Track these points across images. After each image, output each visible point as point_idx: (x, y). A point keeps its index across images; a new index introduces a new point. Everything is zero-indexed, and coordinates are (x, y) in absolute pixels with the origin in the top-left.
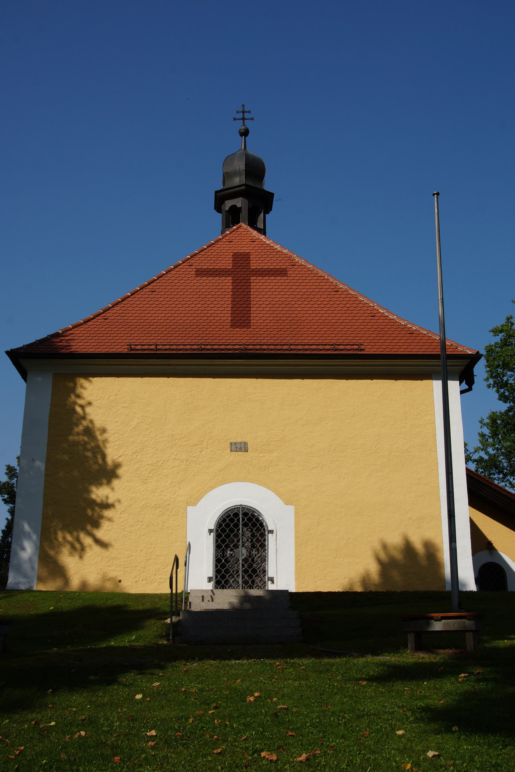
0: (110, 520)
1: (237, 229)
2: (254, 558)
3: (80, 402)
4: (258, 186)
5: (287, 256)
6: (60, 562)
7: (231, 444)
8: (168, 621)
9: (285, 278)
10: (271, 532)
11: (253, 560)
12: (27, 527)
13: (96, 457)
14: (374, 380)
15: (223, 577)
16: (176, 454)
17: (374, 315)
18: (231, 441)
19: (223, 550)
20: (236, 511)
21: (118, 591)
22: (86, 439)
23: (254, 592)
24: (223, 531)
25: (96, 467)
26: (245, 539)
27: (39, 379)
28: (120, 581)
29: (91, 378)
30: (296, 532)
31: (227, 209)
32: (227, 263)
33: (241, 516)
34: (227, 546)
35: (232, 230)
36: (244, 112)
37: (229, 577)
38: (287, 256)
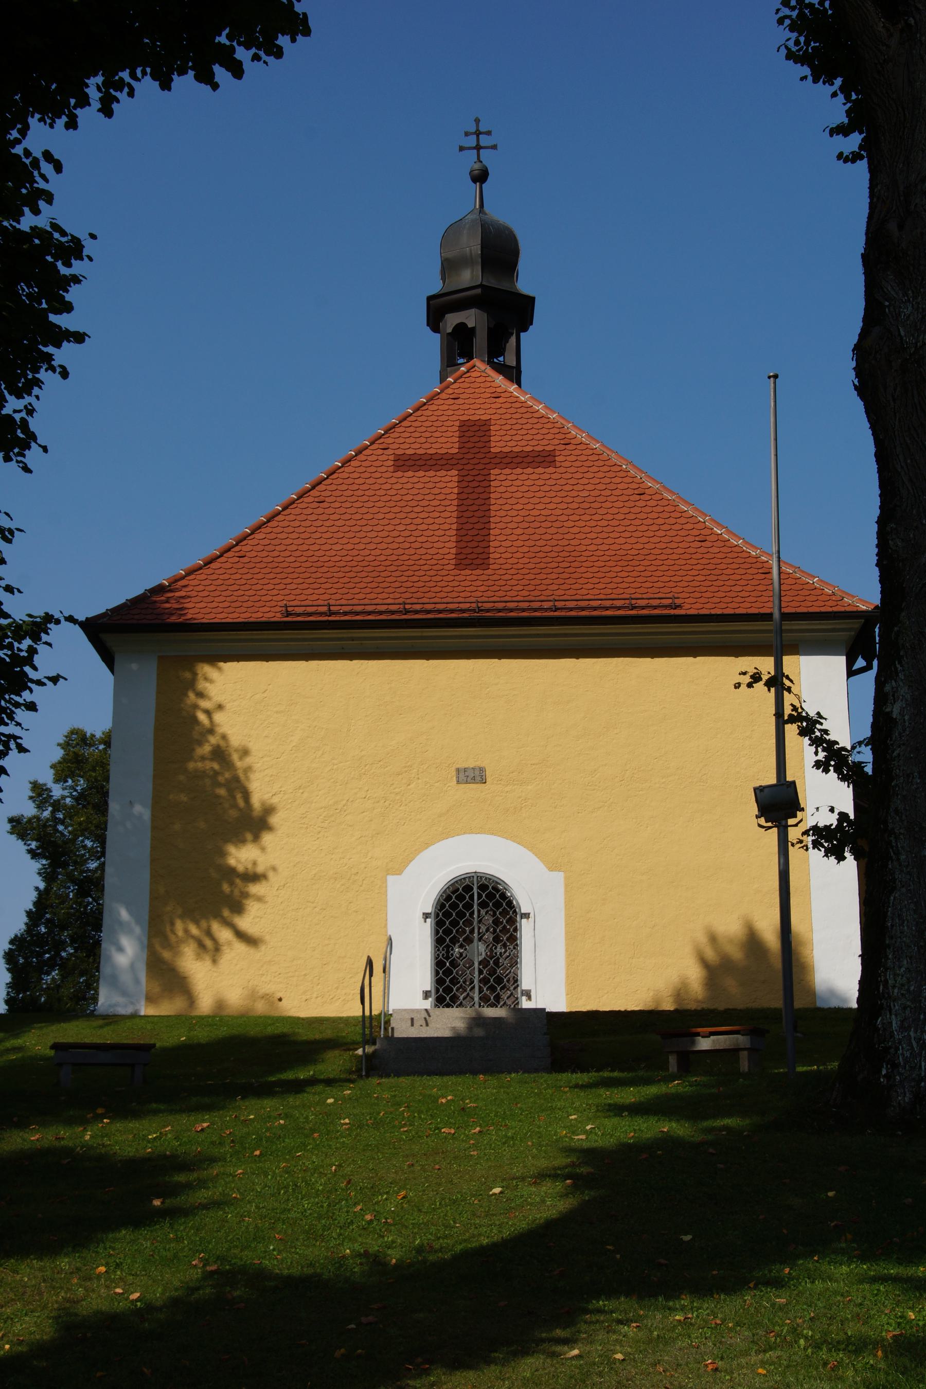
0: (260, 899)
1: (468, 372)
2: (498, 959)
3: (204, 704)
4: (504, 285)
5: (556, 425)
6: (181, 970)
7: (458, 770)
8: (360, 1052)
9: (551, 470)
10: (527, 916)
11: (497, 963)
12: (124, 914)
13: (234, 798)
14: (699, 658)
15: (448, 990)
16: (366, 788)
17: (704, 537)
18: (458, 766)
19: (448, 946)
20: (467, 882)
21: (276, 1014)
22: (216, 766)
23: (491, 1012)
24: (447, 915)
25: (233, 813)
26: (483, 929)
27: (134, 666)
28: (280, 1000)
29: (221, 664)
30: (568, 916)
31: (449, 330)
32: (448, 443)
33: (475, 890)
34: (454, 941)
35: (458, 374)
36: (478, 133)
37: (457, 990)
38: (556, 425)
